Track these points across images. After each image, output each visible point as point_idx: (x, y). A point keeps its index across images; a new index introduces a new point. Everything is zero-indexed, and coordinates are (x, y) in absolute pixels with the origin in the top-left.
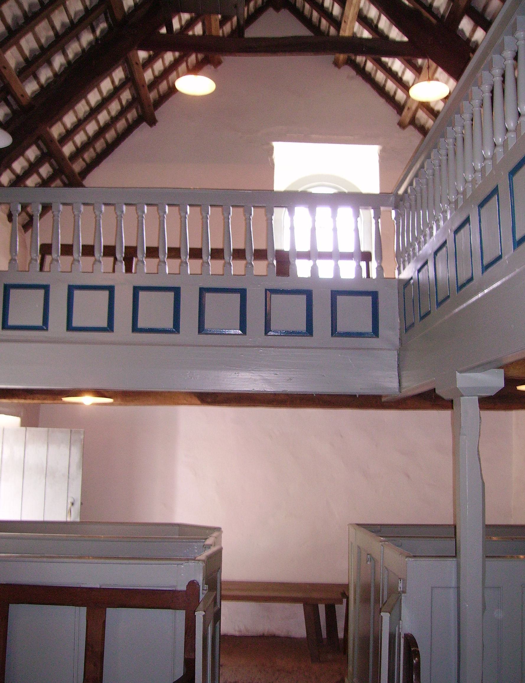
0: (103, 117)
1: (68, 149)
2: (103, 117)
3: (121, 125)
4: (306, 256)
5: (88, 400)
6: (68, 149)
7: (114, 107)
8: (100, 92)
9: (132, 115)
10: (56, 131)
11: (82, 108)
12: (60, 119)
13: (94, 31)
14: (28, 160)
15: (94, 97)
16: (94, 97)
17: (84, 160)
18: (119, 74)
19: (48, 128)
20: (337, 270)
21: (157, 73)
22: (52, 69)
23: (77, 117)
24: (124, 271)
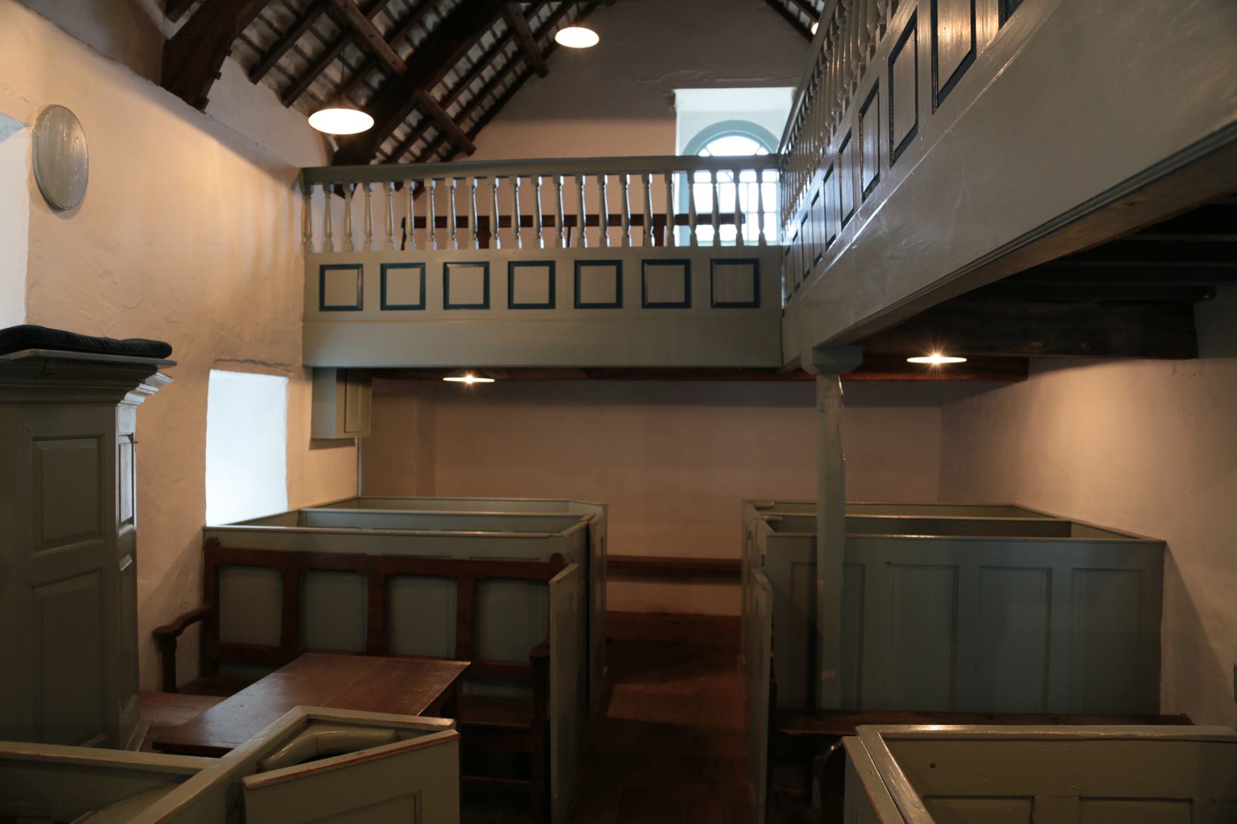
0: (488, 73)
1: (452, 111)
2: (488, 73)
3: (509, 79)
4: (682, 220)
5: (469, 379)
6: (452, 111)
7: (499, 60)
8: (481, 47)
9: (520, 68)
10: (437, 93)
11: (463, 65)
12: (440, 80)
13: (438, 13)
14: (410, 126)
15: (475, 54)
16: (475, 54)
17: (471, 119)
18: (500, 26)
19: (426, 92)
20: (693, 237)
21: (544, 20)
22: (412, 45)
23: (458, 76)
24: (477, 247)
